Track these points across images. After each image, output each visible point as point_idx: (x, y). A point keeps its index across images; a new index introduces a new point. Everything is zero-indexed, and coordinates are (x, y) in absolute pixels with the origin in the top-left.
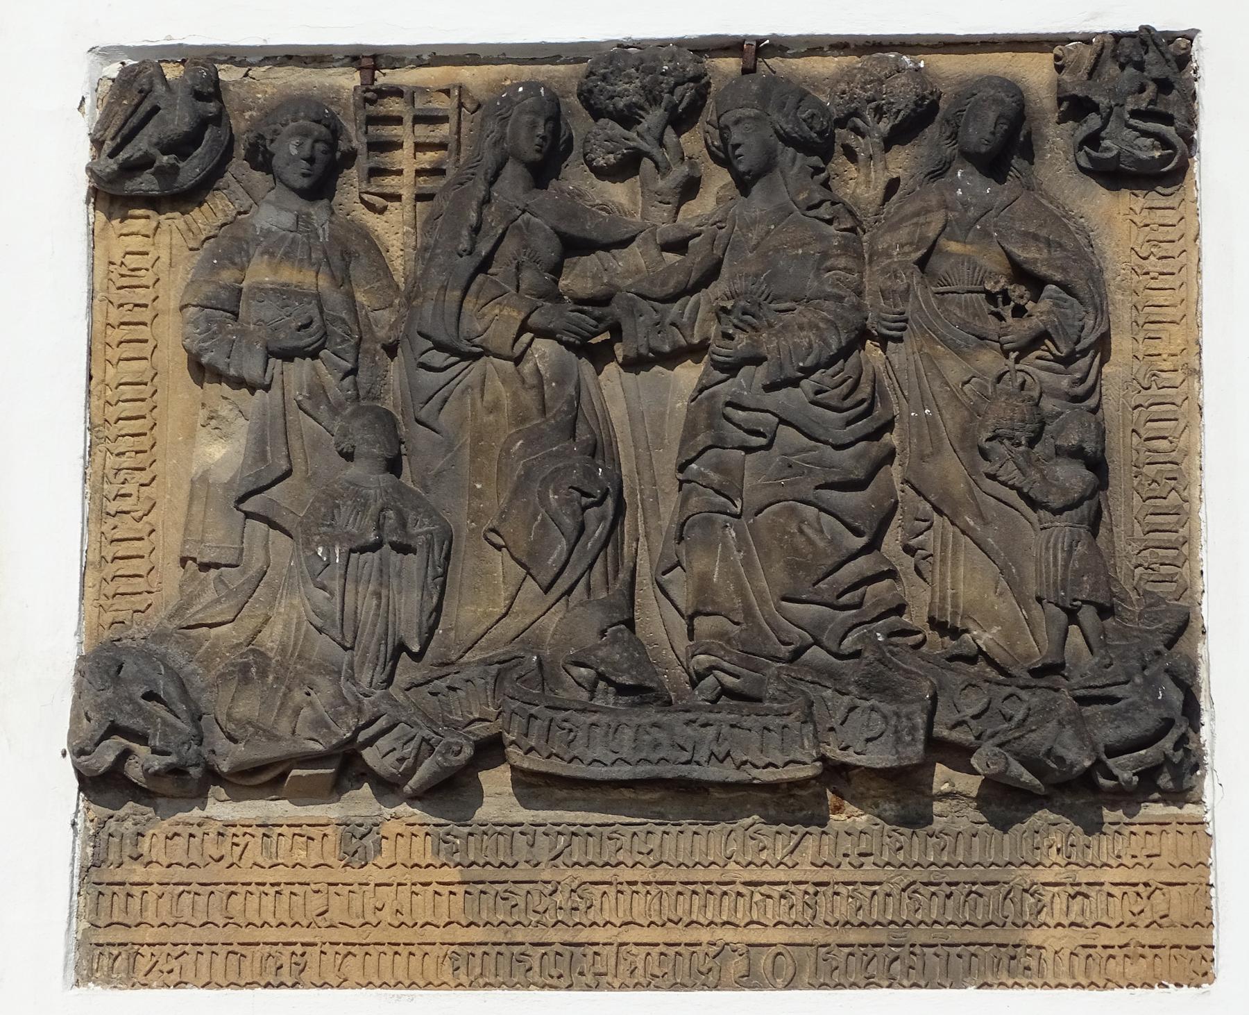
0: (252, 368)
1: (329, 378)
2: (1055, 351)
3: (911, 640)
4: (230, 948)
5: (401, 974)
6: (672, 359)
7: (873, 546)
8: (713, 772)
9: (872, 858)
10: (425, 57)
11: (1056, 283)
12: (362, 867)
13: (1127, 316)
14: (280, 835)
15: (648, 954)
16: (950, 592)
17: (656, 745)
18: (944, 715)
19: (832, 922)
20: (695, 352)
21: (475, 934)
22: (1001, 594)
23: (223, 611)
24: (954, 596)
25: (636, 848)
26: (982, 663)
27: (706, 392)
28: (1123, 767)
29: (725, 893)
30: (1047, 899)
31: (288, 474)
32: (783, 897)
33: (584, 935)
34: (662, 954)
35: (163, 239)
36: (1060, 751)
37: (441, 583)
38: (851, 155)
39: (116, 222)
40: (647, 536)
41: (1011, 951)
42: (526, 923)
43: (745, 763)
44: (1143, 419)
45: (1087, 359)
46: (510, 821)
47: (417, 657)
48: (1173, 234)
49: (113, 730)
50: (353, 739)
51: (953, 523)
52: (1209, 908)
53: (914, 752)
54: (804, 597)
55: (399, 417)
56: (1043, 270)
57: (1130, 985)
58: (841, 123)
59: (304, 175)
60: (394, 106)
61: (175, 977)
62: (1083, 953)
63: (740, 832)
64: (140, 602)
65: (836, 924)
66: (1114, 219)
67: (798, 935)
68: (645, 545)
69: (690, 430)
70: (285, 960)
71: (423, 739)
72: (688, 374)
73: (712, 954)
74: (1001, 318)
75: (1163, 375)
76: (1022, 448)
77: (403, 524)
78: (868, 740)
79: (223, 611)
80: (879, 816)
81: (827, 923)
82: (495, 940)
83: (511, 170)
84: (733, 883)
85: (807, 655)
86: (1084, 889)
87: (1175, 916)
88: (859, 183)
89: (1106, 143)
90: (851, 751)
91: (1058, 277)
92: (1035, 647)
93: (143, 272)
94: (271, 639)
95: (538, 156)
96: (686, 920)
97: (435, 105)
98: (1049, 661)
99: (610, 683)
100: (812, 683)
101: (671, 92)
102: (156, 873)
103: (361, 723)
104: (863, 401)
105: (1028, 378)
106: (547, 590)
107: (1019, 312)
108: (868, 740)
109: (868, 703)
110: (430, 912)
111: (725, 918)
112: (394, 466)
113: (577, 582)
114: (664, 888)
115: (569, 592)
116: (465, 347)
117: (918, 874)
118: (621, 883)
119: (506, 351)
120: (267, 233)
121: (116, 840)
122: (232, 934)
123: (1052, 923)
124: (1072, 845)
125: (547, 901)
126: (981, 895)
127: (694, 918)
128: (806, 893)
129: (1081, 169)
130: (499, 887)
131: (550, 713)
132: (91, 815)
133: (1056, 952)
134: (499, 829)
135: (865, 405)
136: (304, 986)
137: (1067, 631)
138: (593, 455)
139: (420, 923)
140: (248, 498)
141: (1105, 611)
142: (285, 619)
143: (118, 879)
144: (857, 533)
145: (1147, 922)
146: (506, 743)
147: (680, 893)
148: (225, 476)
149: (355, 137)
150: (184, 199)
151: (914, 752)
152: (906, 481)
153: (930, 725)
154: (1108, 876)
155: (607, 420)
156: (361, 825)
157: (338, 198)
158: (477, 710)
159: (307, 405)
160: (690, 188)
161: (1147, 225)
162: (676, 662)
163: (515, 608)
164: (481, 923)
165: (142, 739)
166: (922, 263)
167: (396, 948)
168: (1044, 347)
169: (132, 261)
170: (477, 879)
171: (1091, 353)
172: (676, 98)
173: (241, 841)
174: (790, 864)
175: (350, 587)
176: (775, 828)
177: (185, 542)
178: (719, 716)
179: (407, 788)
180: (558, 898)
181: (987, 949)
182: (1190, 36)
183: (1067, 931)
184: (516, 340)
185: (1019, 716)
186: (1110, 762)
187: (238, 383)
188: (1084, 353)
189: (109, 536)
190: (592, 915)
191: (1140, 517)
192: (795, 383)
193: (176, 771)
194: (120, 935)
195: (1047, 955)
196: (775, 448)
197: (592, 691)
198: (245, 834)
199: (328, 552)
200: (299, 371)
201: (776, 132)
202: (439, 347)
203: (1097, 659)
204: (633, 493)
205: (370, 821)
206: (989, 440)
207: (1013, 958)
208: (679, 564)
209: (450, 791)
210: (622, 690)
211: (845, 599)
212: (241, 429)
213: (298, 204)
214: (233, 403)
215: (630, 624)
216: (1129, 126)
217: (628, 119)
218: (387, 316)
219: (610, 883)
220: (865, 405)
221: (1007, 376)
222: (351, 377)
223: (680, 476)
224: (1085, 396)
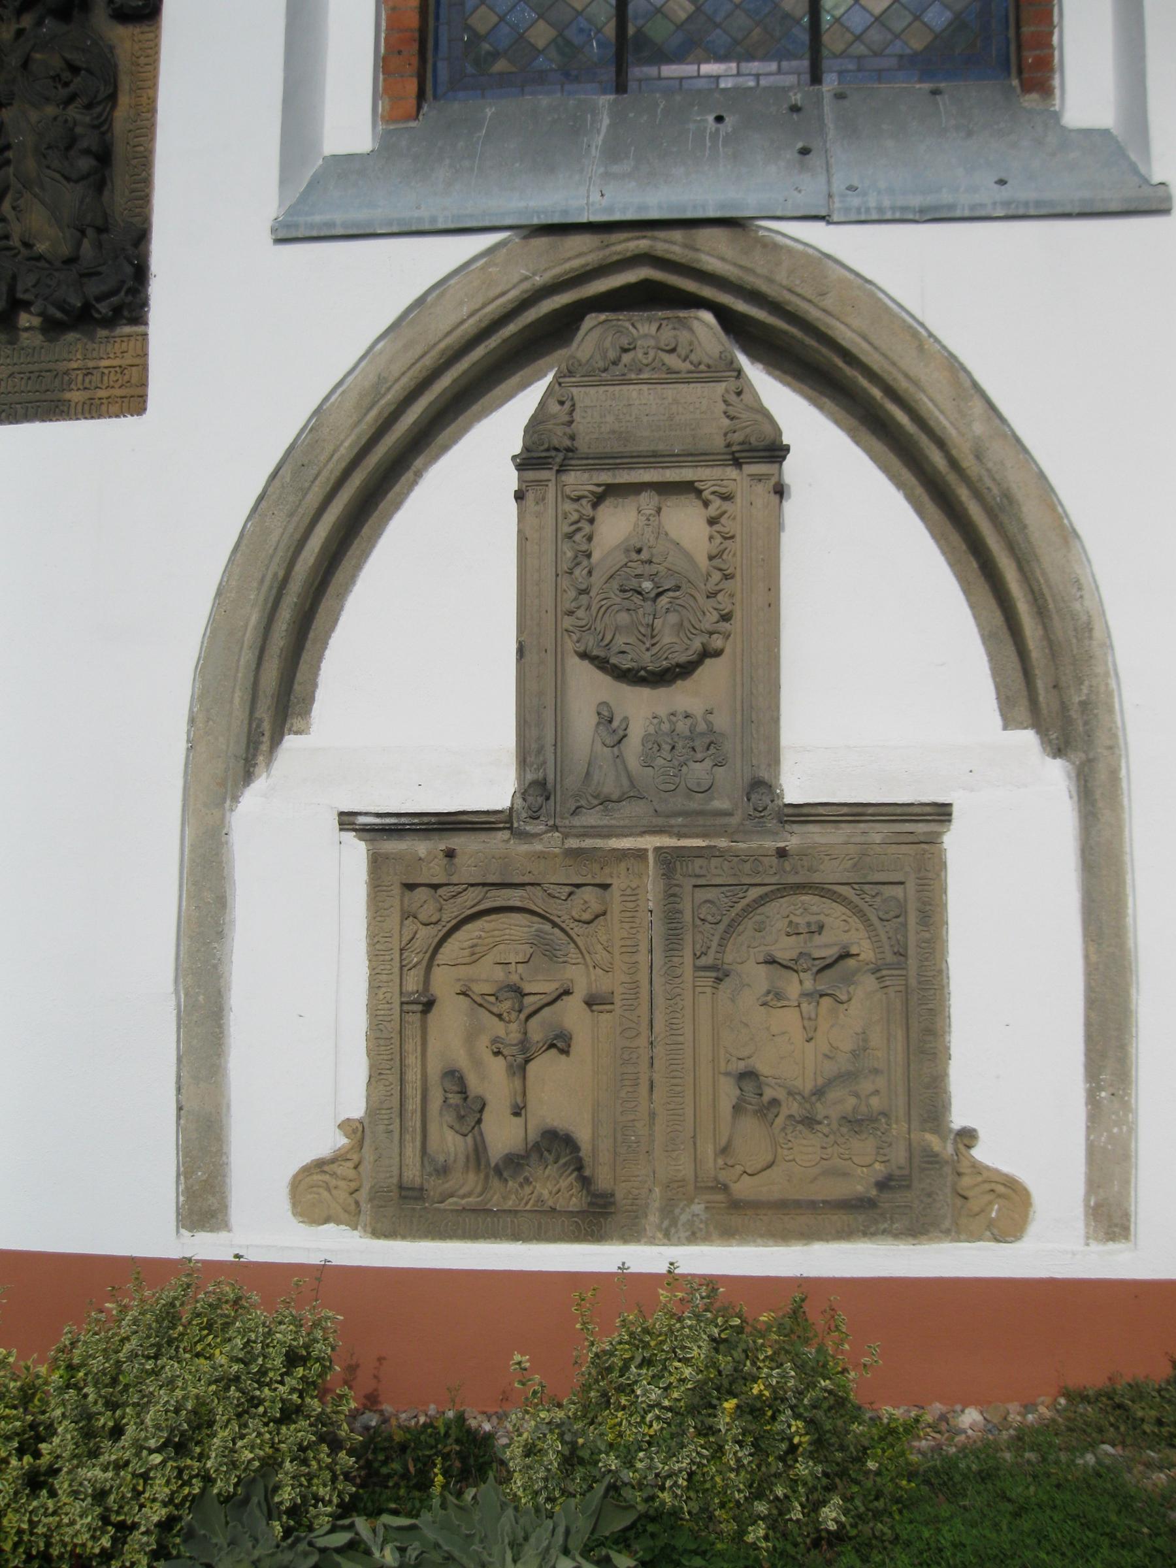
66: (122, 37)
74: (56, 88)
91: (84, 66)
92: (65, 250)
117: (16, 369)
141: (100, 230)
188: (99, 103)
195: (73, 404)
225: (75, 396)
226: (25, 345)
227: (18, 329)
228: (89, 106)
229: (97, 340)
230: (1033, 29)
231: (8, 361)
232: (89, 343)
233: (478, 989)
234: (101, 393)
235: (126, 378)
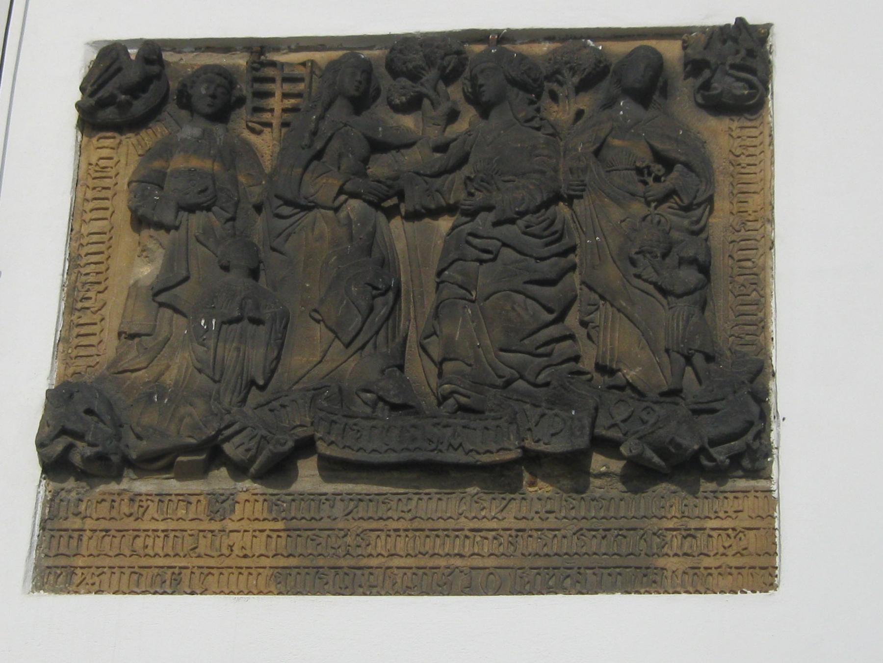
0: (168, 217)
1: (217, 224)
2: (680, 203)
3: (584, 377)
4: (132, 570)
5: (242, 586)
6: (435, 213)
7: (560, 319)
8: (452, 457)
9: (554, 515)
10: (293, 47)
11: (682, 163)
12: (222, 520)
13: (726, 190)
14: (170, 500)
15: (405, 574)
16: (609, 347)
17: (414, 439)
18: (603, 420)
19: (527, 554)
20: (451, 210)
21: (293, 562)
22: (642, 348)
23: (142, 362)
24: (612, 349)
25: (400, 508)
26: (628, 391)
27: (456, 231)
28: (720, 453)
29: (457, 536)
30: (668, 539)
31: (186, 279)
32: (495, 538)
33: (364, 562)
34: (414, 574)
35: (123, 149)
36: (679, 440)
37: (280, 346)
38: (554, 97)
39: (94, 140)
40: (415, 318)
41: (644, 571)
42: (326, 554)
43: (471, 451)
44: (736, 249)
45: (701, 210)
46: (319, 491)
47: (262, 388)
48: (756, 142)
49: (64, 432)
50: (215, 437)
51: (612, 305)
52: (775, 544)
53: (582, 442)
54: (514, 348)
55: (261, 248)
56: (673, 155)
57: (722, 592)
58: (548, 78)
59: (209, 105)
60: (270, 72)
61: (96, 587)
62: (691, 572)
63: (468, 498)
64: (91, 361)
65: (530, 555)
66: (718, 134)
67: (503, 562)
68: (413, 321)
69: (446, 251)
70: (168, 577)
71: (263, 437)
72: (445, 224)
73: (446, 574)
74: (645, 183)
75: (749, 223)
76: (659, 259)
77: (257, 307)
78: (553, 435)
79: (142, 362)
80: (560, 489)
81: (523, 554)
82: (305, 565)
83: (340, 103)
84: (462, 530)
85: (515, 385)
86: (692, 532)
87: (752, 549)
88: (560, 113)
89: (715, 85)
90: (541, 443)
91: (683, 158)
92: (663, 380)
93: (109, 169)
94: (169, 378)
95: (357, 94)
96: (431, 552)
97: (296, 72)
98: (672, 387)
99: (386, 402)
100: (517, 400)
101: (443, 59)
102: (89, 524)
103: (222, 427)
104: (556, 232)
105: (663, 220)
106: (347, 345)
107: (657, 179)
108: (553, 435)
109: (554, 412)
110: (263, 548)
111: (456, 551)
112: (254, 274)
113: (368, 342)
114: (417, 533)
115: (362, 347)
116: (303, 202)
117: (584, 524)
118: (389, 530)
119: (329, 203)
120: (184, 140)
121: (65, 503)
122: (136, 561)
123: (671, 553)
124: (686, 505)
125: (340, 542)
126: (625, 537)
127: (436, 551)
128: (510, 536)
129: (699, 105)
130: (309, 533)
131: (345, 420)
132: (50, 488)
133: (674, 572)
134: (312, 497)
135: (557, 235)
136: (180, 593)
137: (684, 370)
138: (382, 267)
139: (257, 554)
140: (161, 294)
141: (709, 358)
142: (177, 366)
143: (64, 527)
144: (550, 311)
145: (734, 552)
146: (316, 438)
147: (428, 536)
148: (148, 282)
149: (244, 88)
150: (136, 125)
151: (582, 442)
152: (583, 283)
153: (593, 425)
154: (710, 524)
155: (393, 247)
156: (222, 495)
157: (231, 125)
158: (298, 421)
159: (202, 238)
160: (453, 116)
161: (739, 137)
162: (431, 394)
163: (327, 358)
164: (297, 555)
165: (80, 437)
166: (597, 153)
167: (240, 570)
168: (672, 200)
169: (103, 163)
170: (295, 527)
171: (703, 206)
172: (445, 63)
173: (144, 504)
174: (500, 518)
175: (220, 344)
176: (491, 496)
177: (122, 323)
178: (455, 421)
179: (252, 470)
180: (348, 539)
181: (628, 570)
182: (768, 27)
183: (682, 559)
184: (336, 198)
185: (652, 421)
186: (712, 451)
187: (160, 226)
188: (699, 205)
189: (75, 322)
190: (370, 550)
191: (733, 307)
192: (512, 221)
193: (102, 458)
194: (63, 561)
196: (499, 261)
197: (374, 406)
198: (147, 500)
199: (208, 323)
200: (197, 220)
201: (506, 76)
202: (288, 203)
203: (704, 387)
204: (408, 292)
205: (228, 492)
206: (637, 253)
207: (645, 576)
208: (435, 333)
209: (278, 470)
210: (394, 407)
211: (541, 350)
212: (160, 255)
213: (205, 124)
214: (157, 240)
215: (401, 368)
216: (730, 75)
217: (414, 76)
218: (257, 190)
219: (382, 530)
220: (557, 235)
221: (649, 218)
222: (231, 223)
223: (438, 280)
224: (698, 231)
225: (672, 563)
226: (597, 495)
227: (588, 474)
228: (687, 209)
229: (700, 494)
230: (471, 115)
231: (573, 513)
232: (690, 497)
233: (237, 505)
234: (706, 562)
235: (743, 544)
